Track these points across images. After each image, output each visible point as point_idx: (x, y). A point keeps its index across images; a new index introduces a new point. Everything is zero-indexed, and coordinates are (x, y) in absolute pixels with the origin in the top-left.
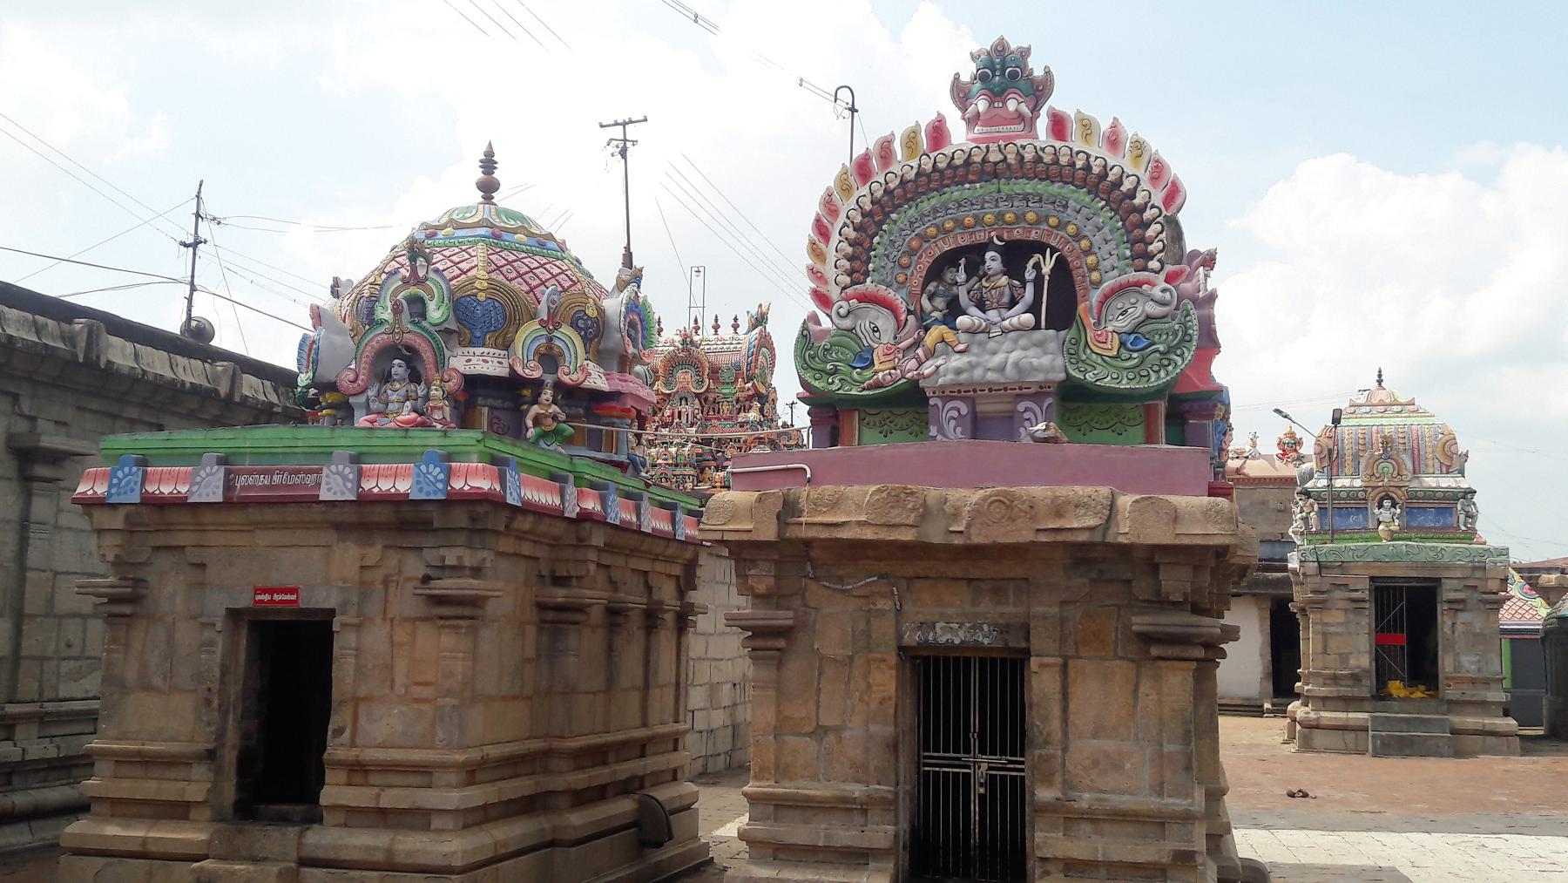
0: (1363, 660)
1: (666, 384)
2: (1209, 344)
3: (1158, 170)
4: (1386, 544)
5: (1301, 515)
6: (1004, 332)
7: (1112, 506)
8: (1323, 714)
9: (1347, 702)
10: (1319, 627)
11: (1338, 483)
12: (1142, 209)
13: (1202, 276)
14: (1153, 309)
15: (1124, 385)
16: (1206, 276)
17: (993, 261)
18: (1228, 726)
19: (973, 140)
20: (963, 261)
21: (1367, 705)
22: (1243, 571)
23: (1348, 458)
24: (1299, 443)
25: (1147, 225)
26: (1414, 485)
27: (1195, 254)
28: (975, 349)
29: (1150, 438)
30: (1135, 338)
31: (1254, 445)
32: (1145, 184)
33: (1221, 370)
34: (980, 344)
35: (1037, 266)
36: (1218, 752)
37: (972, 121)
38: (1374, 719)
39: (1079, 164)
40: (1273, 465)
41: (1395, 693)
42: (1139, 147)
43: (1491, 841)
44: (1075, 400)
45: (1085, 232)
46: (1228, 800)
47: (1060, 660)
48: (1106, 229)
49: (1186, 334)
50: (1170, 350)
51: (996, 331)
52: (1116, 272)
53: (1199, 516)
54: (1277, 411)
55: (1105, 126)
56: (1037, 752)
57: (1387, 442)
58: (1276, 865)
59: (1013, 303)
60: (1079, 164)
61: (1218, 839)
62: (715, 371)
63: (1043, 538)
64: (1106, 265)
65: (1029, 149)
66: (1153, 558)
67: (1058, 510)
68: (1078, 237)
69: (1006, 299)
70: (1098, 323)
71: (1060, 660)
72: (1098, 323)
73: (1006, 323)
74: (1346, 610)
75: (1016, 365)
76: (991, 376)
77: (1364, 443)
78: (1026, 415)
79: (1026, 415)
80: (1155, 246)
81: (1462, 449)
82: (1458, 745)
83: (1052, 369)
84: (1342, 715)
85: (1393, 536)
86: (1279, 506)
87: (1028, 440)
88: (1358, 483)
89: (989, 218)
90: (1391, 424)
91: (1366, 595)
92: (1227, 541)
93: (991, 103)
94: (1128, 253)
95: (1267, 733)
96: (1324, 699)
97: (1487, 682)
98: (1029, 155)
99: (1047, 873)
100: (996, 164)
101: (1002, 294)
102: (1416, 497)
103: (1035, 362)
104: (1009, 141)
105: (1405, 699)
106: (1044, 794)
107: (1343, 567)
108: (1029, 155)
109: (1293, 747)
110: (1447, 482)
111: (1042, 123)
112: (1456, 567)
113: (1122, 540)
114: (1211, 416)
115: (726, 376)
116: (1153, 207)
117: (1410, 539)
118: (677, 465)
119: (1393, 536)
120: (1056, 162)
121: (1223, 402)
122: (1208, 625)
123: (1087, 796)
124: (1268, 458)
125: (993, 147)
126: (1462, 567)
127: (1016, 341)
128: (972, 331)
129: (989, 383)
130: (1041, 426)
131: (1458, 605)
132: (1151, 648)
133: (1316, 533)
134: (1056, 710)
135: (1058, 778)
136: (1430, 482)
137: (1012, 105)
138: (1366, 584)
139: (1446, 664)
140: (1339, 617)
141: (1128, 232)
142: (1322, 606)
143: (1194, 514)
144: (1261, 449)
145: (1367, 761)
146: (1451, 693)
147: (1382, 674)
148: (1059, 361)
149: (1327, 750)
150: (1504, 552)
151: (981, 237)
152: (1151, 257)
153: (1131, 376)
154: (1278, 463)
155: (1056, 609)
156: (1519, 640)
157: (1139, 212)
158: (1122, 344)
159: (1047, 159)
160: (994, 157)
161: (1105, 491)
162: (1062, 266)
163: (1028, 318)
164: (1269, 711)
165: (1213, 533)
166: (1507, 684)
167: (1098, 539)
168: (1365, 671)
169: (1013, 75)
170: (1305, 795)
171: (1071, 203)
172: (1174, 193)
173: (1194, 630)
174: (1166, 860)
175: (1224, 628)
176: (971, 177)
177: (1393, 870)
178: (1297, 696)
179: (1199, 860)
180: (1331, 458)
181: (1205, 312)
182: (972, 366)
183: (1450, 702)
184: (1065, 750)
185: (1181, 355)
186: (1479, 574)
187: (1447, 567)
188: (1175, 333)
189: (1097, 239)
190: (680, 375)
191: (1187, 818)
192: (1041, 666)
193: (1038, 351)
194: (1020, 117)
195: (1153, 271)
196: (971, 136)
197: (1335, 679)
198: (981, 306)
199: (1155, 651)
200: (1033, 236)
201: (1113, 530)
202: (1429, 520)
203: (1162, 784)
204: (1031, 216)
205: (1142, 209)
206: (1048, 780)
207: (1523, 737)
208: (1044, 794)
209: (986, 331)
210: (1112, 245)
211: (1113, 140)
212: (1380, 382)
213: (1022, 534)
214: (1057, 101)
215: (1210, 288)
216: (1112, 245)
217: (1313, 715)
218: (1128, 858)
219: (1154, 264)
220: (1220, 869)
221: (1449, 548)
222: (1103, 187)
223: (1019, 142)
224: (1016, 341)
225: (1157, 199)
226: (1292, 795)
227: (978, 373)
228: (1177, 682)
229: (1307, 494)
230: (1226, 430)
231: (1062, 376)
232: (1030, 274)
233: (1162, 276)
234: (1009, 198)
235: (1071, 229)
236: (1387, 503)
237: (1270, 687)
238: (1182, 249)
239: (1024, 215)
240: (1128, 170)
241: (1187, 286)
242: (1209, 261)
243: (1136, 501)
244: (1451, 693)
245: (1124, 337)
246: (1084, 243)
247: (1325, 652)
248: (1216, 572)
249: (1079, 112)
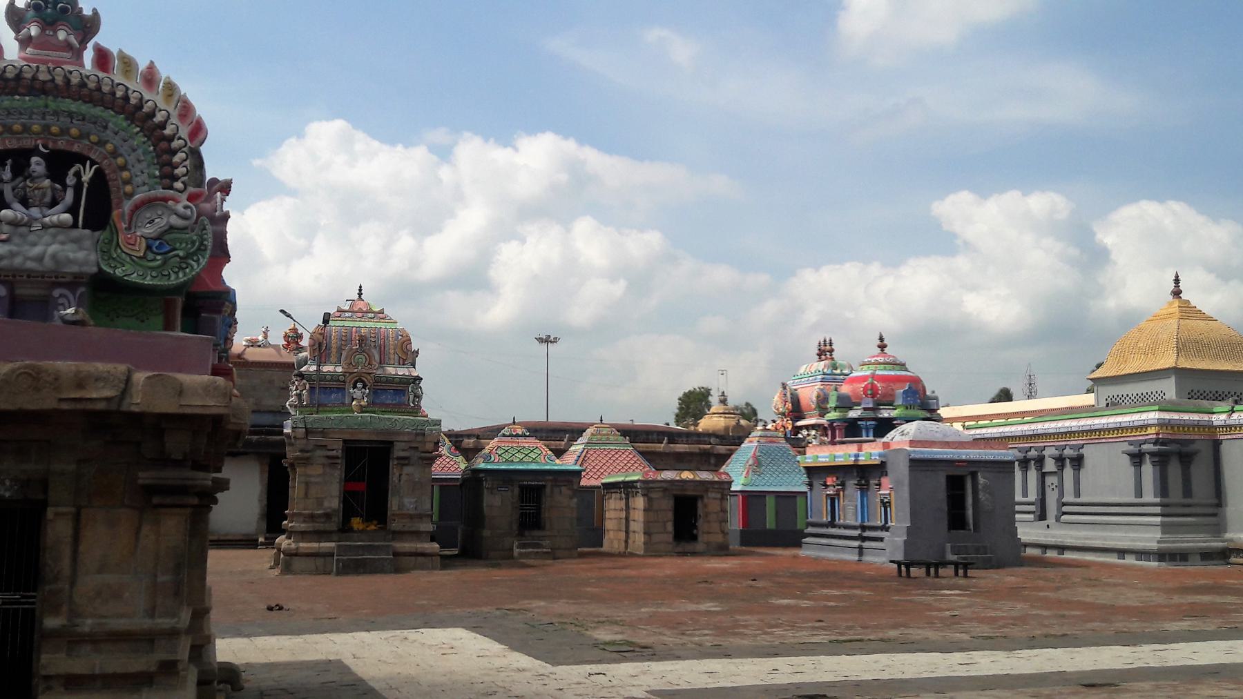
0: (334, 503)
2: (221, 254)
3: (186, 109)
4: (357, 414)
5: (296, 392)
6: (45, 227)
7: (128, 381)
8: (301, 545)
9: (320, 535)
10: (303, 479)
11: (326, 368)
12: (170, 139)
13: (219, 199)
14: (175, 220)
15: (148, 281)
16: (223, 200)
17: (37, 165)
18: (216, 559)
19: (24, 59)
20: (9, 162)
21: (335, 537)
22: (238, 434)
23: (334, 350)
24: (301, 337)
25: (174, 152)
27: (214, 181)
28: (16, 240)
29: (168, 326)
30: (161, 243)
31: (266, 337)
32: (174, 119)
33: (231, 275)
34: (22, 236)
35: (78, 175)
36: (205, 579)
37: (25, 42)
38: (339, 546)
39: (119, 94)
41: (355, 527)
42: (171, 88)
43: (411, 634)
44: (106, 293)
45: (122, 151)
46: (213, 615)
47: (73, 510)
48: (140, 151)
49: (202, 244)
50: (189, 256)
51: (37, 226)
52: (146, 188)
53: (200, 391)
54: (282, 311)
55: (142, 65)
56: (47, 588)
57: (362, 339)
58: (249, 665)
59: (54, 203)
60: (119, 94)
61: (201, 648)
63: (65, 406)
64: (139, 180)
65: (75, 74)
66: (159, 424)
67: (80, 383)
68: (115, 154)
69: (48, 199)
70: (129, 228)
71: (73, 510)
72: (129, 228)
73: (47, 219)
74: (324, 465)
75: (54, 257)
76: (30, 265)
77: (346, 338)
78: (61, 301)
79: (61, 301)
80: (181, 170)
81: (414, 347)
82: (398, 564)
83: (86, 263)
84: (315, 545)
85: (362, 410)
86: (282, 385)
87: (59, 323)
88: (339, 369)
89: (36, 128)
90: (366, 326)
91: (339, 453)
92: (222, 411)
93: (43, 30)
94: (157, 173)
95: (260, 561)
97: (420, 517)
98: (75, 80)
99: (49, 688)
100: (44, 82)
101: (44, 195)
102: (325, 380)
103: (71, 255)
104: (58, 65)
105: (362, 531)
106: (52, 622)
107: (324, 432)
108: (75, 80)
109: (276, 572)
110: (402, 371)
111: (88, 56)
112: (404, 434)
113: (135, 409)
114: (219, 312)
116: (180, 138)
117: (374, 412)
119: (362, 410)
120: (99, 89)
121: (230, 302)
122: (205, 479)
123: (89, 621)
124: (276, 347)
125: (43, 68)
126: (409, 433)
127: (54, 236)
128: (14, 224)
129: (27, 270)
130: (71, 311)
132: (151, 500)
133: (306, 406)
134: (67, 551)
135: (65, 608)
136: (391, 370)
137: (62, 35)
138: (340, 445)
139: (393, 504)
140: (320, 470)
141: (158, 156)
142: (306, 461)
143: (197, 388)
144: (271, 340)
145: (332, 579)
146: (395, 525)
147: (349, 510)
148: (93, 257)
149: (302, 572)
150: (438, 423)
151: (28, 143)
152: (176, 179)
153: (154, 274)
154: (283, 351)
155: (73, 467)
156: (446, 486)
157: (164, 140)
158: (149, 248)
159: (92, 85)
160: (43, 76)
161: (122, 368)
162: (99, 176)
163: (67, 217)
164: (262, 544)
165: (212, 405)
166: (435, 518)
167: (113, 407)
168: (334, 511)
169: (64, 10)
170: (281, 608)
171: (110, 125)
172: (198, 130)
173: (190, 483)
174: (153, 669)
175: (215, 480)
176: (21, 90)
177: (339, 662)
178: (283, 532)
179: (180, 667)
180: (321, 348)
181: (218, 228)
182: (12, 255)
183: (394, 532)
184: (73, 584)
185: (197, 261)
186: (419, 439)
187: (398, 433)
188: (193, 243)
189: (131, 159)
191: (173, 634)
192: (57, 514)
193: (74, 246)
194: (68, 46)
195: (177, 190)
196: (23, 55)
197: (312, 517)
198: (25, 203)
199: (156, 500)
200: (76, 148)
201: (127, 401)
202: (388, 399)
203: (154, 608)
204: (74, 131)
205: (170, 139)
206: (55, 611)
207: (442, 557)
208: (52, 622)
209: (28, 225)
210: (144, 164)
211: (150, 78)
212: (360, 294)
213: (47, 402)
214: (103, 38)
215: (225, 209)
216: (144, 164)
217: (293, 546)
218: (119, 670)
219: (179, 185)
220: (201, 673)
221: (400, 419)
222: (137, 114)
223: (68, 67)
224: (54, 236)
225: (184, 132)
226: (270, 609)
227: (18, 261)
228: (172, 527)
229: (301, 376)
230: (231, 323)
231: (95, 269)
232: (70, 180)
233: (184, 196)
234: (56, 113)
235: (109, 147)
236: (359, 385)
237: (264, 526)
238: (203, 175)
239: (68, 130)
240: (161, 105)
241: (207, 206)
242: (226, 188)
243: (148, 378)
244: (395, 525)
245: (150, 242)
246: (120, 161)
247: (306, 494)
248: (214, 438)
249: (120, 51)
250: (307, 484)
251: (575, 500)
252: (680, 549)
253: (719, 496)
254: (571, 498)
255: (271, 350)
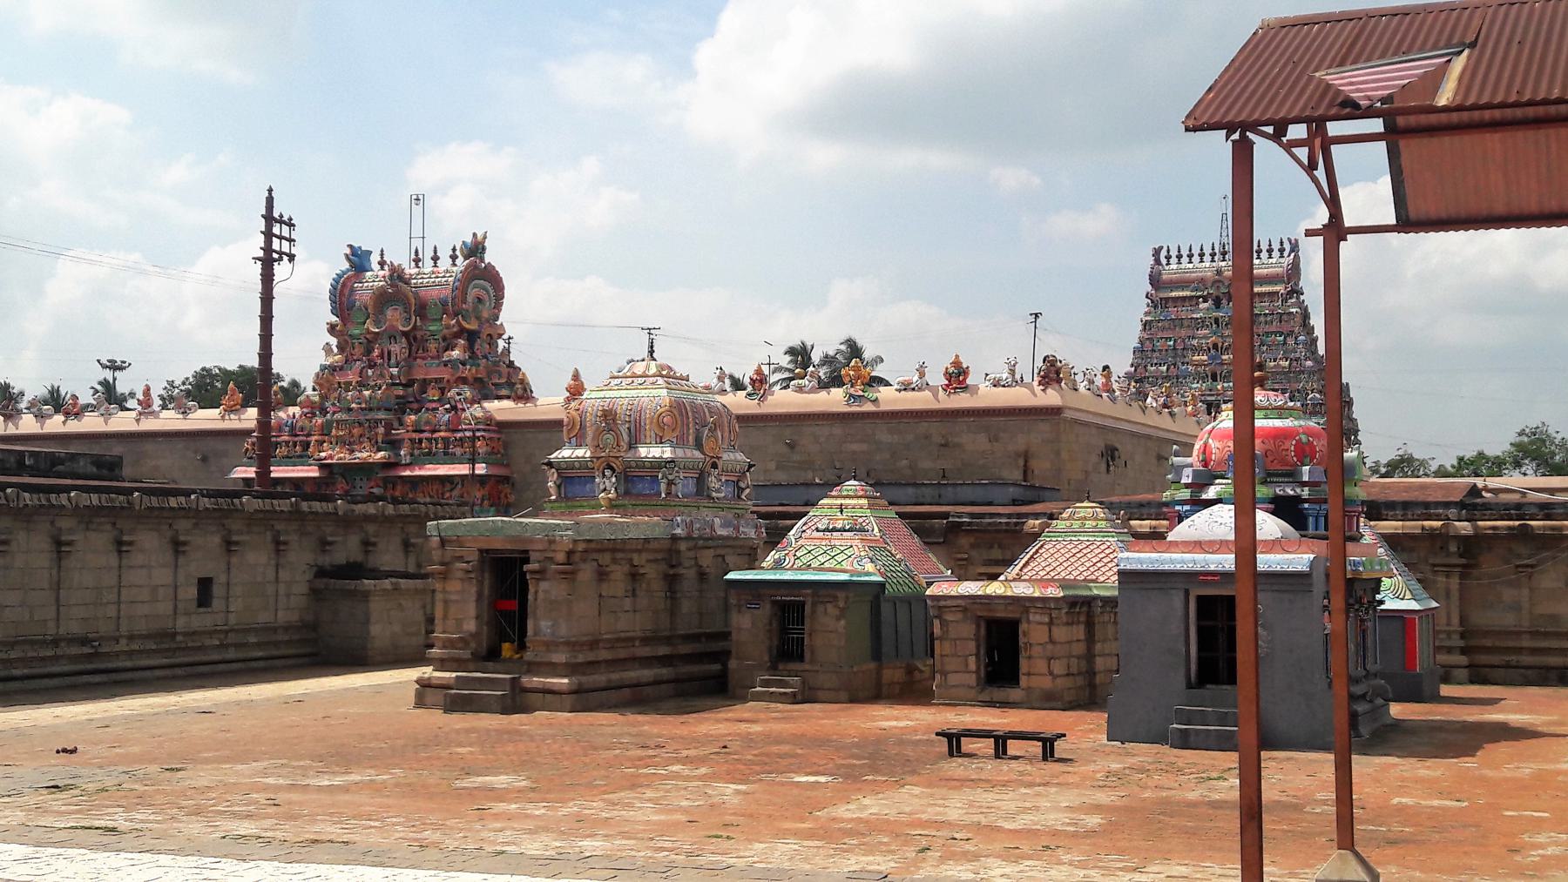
1: (377, 323)
26: (629, 456)
31: (922, 375)
40: (936, 396)
62: (422, 309)
77: (608, 416)
96: (442, 660)
107: (459, 541)
115: (432, 312)
118: (371, 409)
131: (541, 573)
136: (643, 451)
187: (531, 541)
190: (389, 313)
212: (651, 352)
250: (446, 602)
251: (843, 622)
252: (985, 697)
253: (1047, 620)
254: (838, 619)
255: (927, 393)
